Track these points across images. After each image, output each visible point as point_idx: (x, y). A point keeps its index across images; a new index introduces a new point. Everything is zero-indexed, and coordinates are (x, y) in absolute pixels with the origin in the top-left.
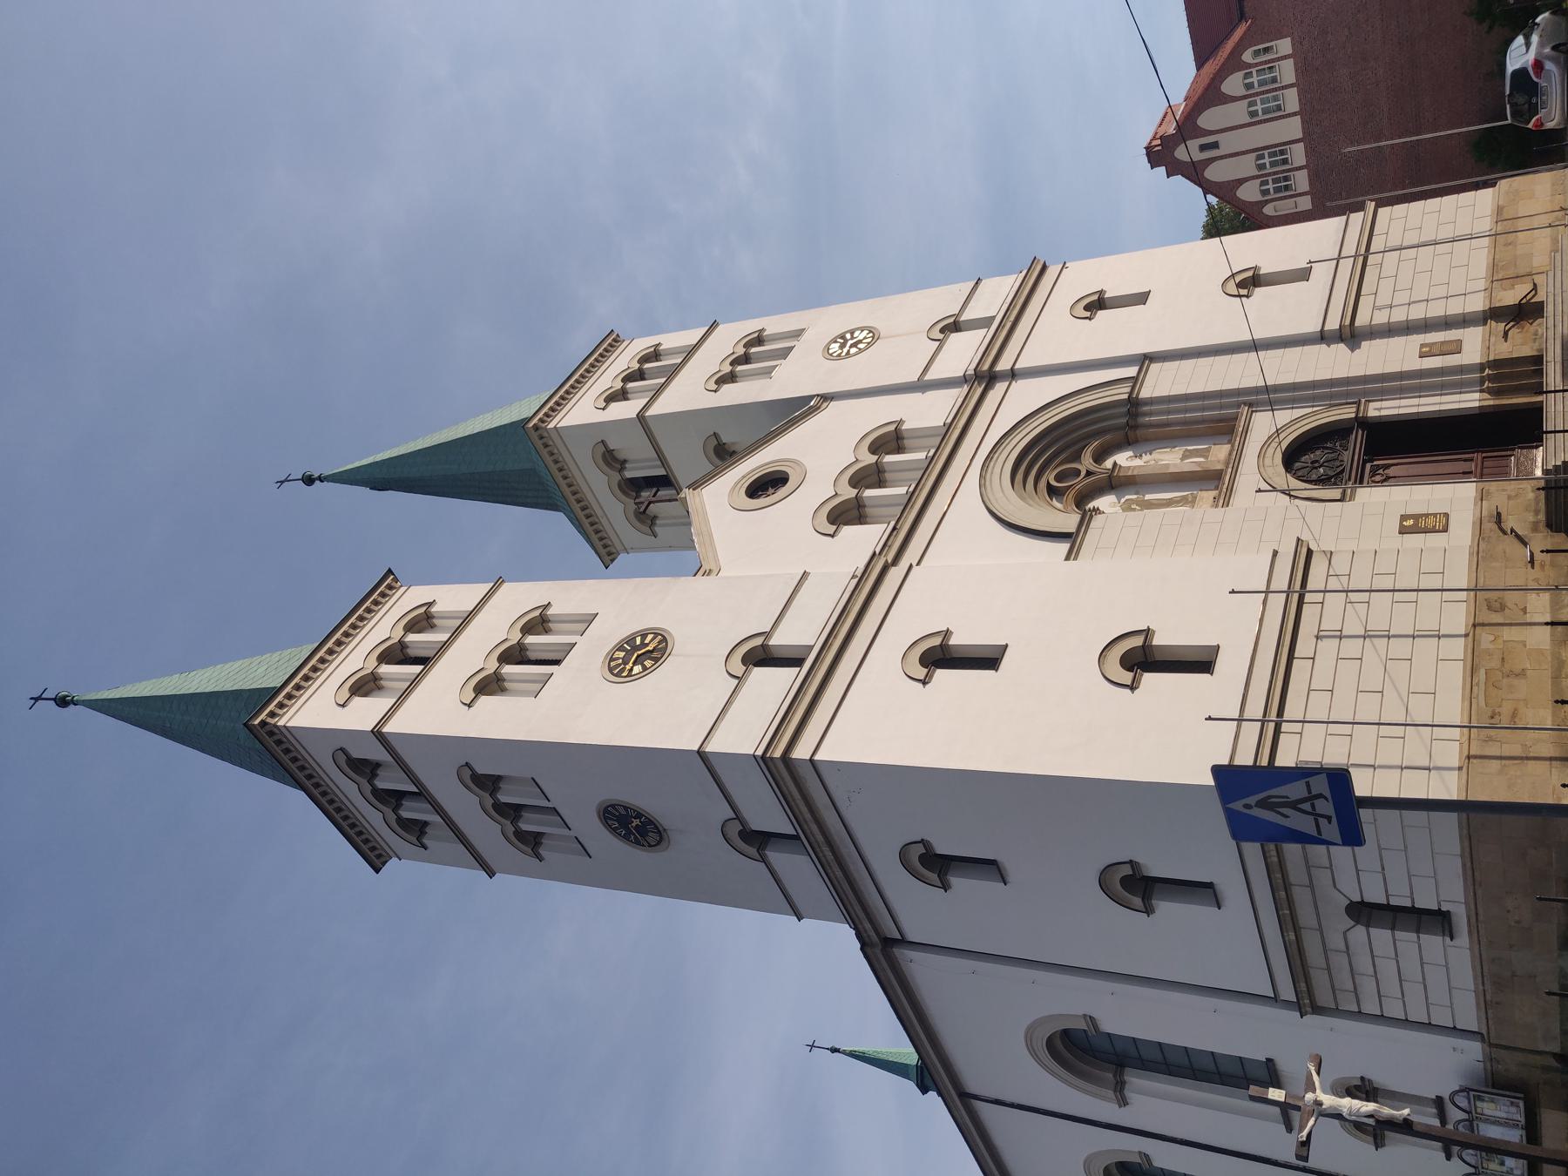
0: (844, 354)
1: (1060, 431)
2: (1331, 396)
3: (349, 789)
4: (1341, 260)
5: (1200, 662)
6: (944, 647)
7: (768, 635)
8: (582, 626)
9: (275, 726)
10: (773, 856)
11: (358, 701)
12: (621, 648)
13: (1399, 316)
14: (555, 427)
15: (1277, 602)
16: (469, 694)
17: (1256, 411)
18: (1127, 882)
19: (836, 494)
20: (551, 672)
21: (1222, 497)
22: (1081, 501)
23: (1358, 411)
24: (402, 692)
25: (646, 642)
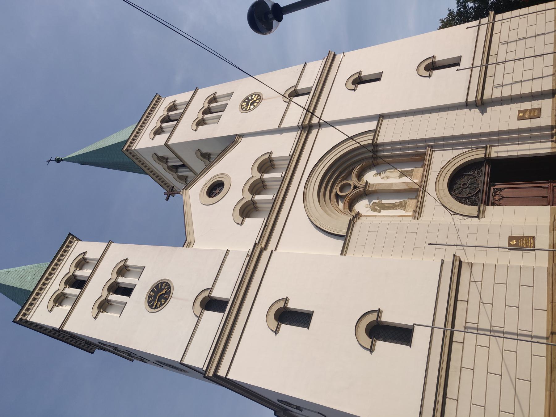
0: (248, 109)
1: (342, 161)
2: (472, 143)
3: (160, 168)
4: (474, 68)
5: (455, 63)
7: (211, 290)
8: (217, 120)
9: (26, 320)
11: (157, 137)
12: (245, 102)
13: (507, 92)
14: (134, 149)
15: (476, 71)
16: (195, 127)
17: (435, 151)
19: (243, 197)
21: (418, 211)
22: (351, 206)
23: (486, 154)
24: (96, 264)
25: (253, 97)
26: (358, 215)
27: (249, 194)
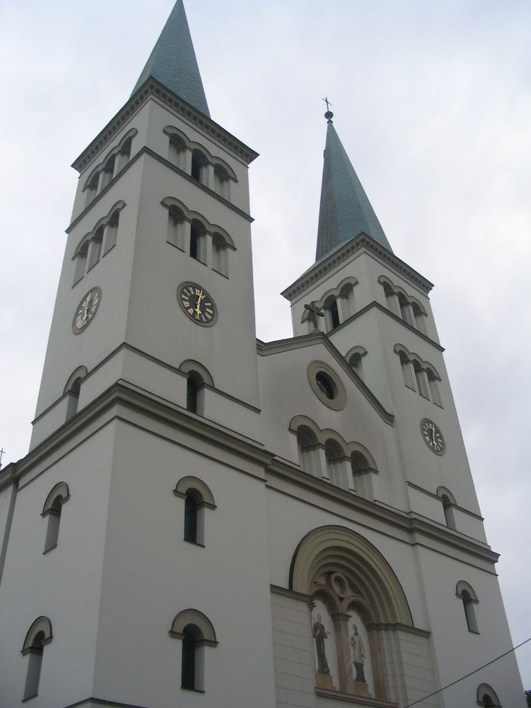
0: (183, 296)
3: (331, 283)
6: (203, 504)
10: (67, 399)
18: (41, 635)
20: (207, 264)
22: (323, 595)
26: (312, 606)
27: (297, 427)
